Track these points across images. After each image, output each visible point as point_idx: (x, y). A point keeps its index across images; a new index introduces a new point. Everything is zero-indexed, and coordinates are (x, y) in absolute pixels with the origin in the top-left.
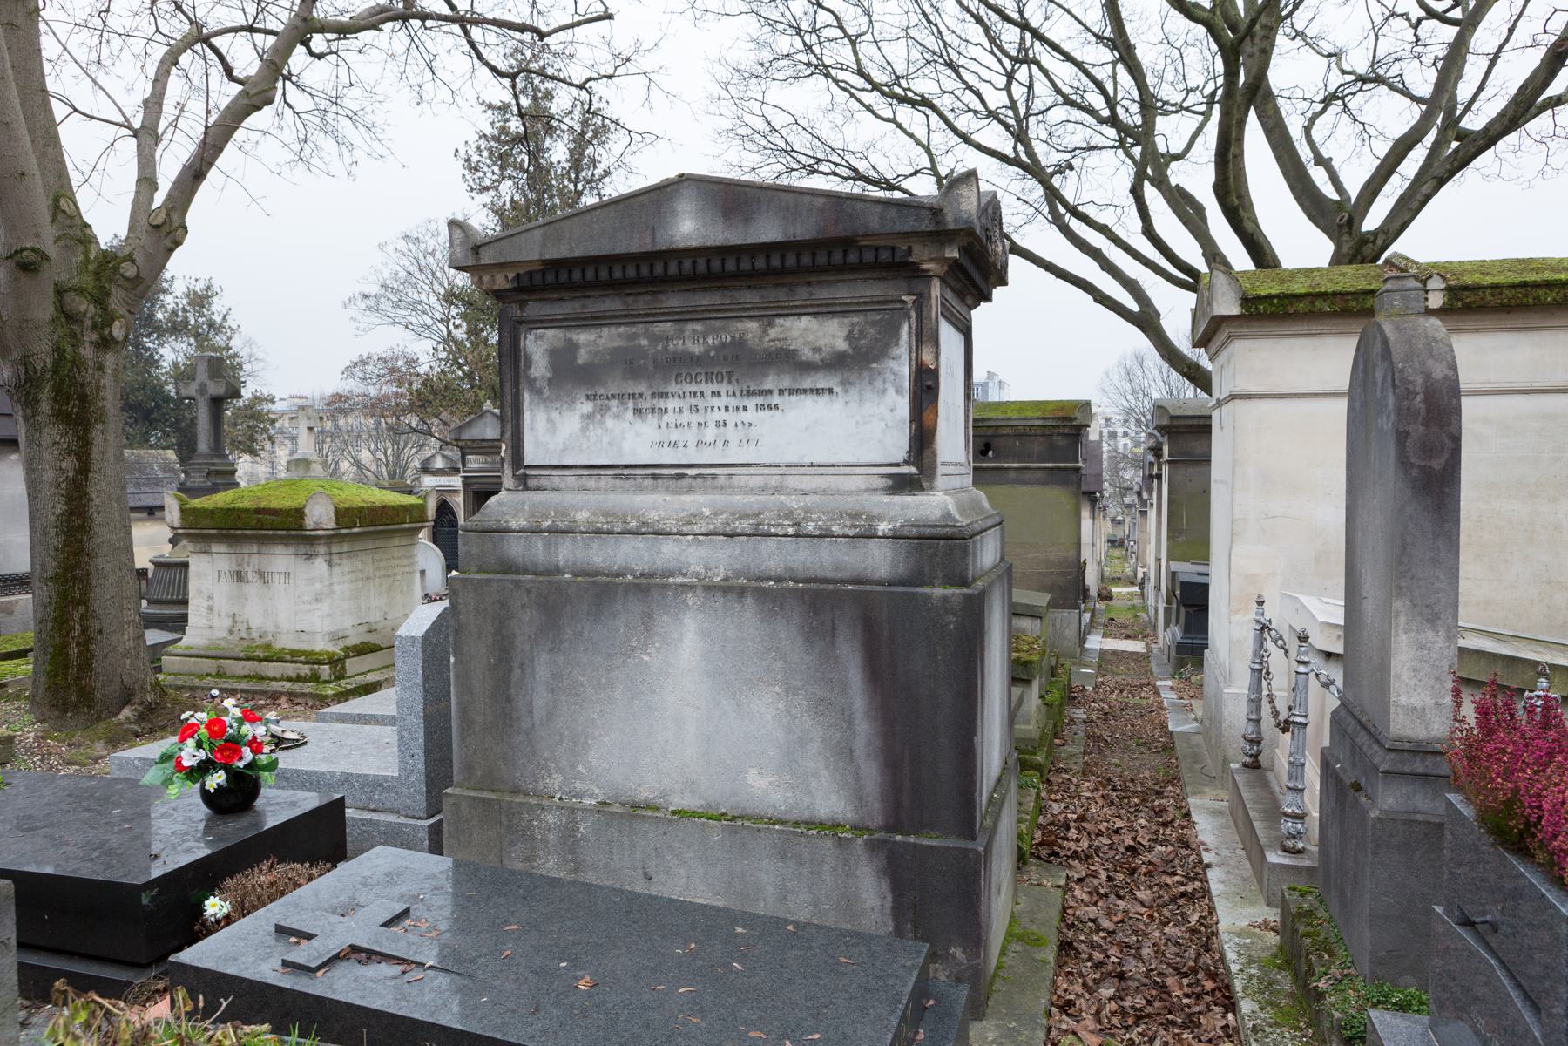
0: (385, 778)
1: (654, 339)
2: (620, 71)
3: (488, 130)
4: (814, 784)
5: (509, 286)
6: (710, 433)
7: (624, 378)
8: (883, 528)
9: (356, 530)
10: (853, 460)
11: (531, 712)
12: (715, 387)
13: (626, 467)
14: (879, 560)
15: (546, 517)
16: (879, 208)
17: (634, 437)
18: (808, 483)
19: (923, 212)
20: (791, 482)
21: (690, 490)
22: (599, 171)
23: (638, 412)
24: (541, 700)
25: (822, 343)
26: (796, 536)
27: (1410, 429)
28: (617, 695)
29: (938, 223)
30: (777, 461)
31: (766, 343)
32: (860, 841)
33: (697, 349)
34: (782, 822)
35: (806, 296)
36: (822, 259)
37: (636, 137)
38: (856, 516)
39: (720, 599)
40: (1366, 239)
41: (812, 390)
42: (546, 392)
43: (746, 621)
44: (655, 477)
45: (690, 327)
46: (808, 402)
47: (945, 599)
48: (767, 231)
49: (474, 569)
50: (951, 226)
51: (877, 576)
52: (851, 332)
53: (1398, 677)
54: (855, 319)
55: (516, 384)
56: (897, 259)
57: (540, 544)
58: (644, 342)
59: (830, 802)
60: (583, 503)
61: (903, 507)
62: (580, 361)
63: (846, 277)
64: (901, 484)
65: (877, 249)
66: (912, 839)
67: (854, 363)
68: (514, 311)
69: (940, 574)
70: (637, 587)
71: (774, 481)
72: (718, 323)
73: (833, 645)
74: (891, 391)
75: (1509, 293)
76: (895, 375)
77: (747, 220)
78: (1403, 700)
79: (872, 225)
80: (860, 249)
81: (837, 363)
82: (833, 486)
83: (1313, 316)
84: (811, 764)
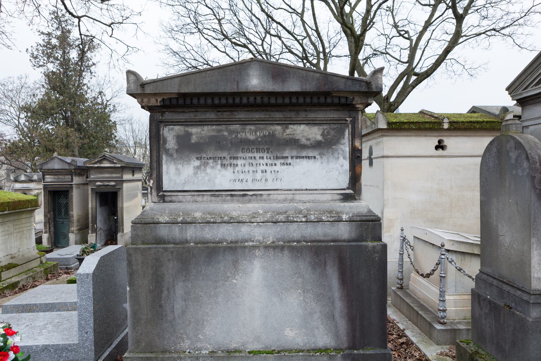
0: (70, 345)
1: (231, 132)
2: (124, 22)
3: (42, 43)
4: (316, 332)
5: (159, 104)
6: (259, 175)
7: (216, 150)
8: (345, 217)
9: (6, 212)
10: (325, 188)
11: (173, 312)
12: (261, 155)
13: (217, 191)
14: (344, 231)
15: (179, 216)
16: (343, 80)
17: (221, 177)
18: (305, 197)
19: (363, 83)
20: (298, 197)
21: (250, 201)
22: (91, 63)
23: (223, 165)
24: (178, 305)
25: (310, 136)
26: (306, 222)
27: (536, 175)
28: (220, 300)
29: (369, 88)
30: (302, 188)
31: (285, 136)
32: (339, 355)
33: (252, 137)
34: (302, 351)
35: (304, 116)
36: (315, 100)
37: (130, 49)
38: (330, 212)
39: (271, 252)
40: (391, 105)
41: (306, 157)
42: (175, 155)
43: (284, 262)
44: (232, 196)
45: (248, 127)
46: (305, 162)
47: (374, 247)
48: (293, 86)
49: (140, 242)
50: (375, 90)
51: (343, 238)
52: (323, 132)
53: (534, 267)
54: (325, 127)
55: (159, 151)
56: (348, 103)
57: (177, 229)
58: (226, 133)
59: (323, 339)
60: (198, 209)
61: (357, 207)
62: (193, 141)
63: (322, 109)
64: (347, 198)
65: (339, 98)
66: (361, 352)
67: (325, 146)
68: (159, 116)
69: (370, 236)
70: (231, 248)
71: (290, 197)
72: (262, 126)
73: (325, 269)
74: (341, 158)
75: (467, 124)
76: (343, 151)
77: (284, 81)
78: (536, 275)
79: (340, 87)
80: (332, 97)
81: (317, 145)
82: (317, 199)
83: (409, 130)
84: (315, 323)
